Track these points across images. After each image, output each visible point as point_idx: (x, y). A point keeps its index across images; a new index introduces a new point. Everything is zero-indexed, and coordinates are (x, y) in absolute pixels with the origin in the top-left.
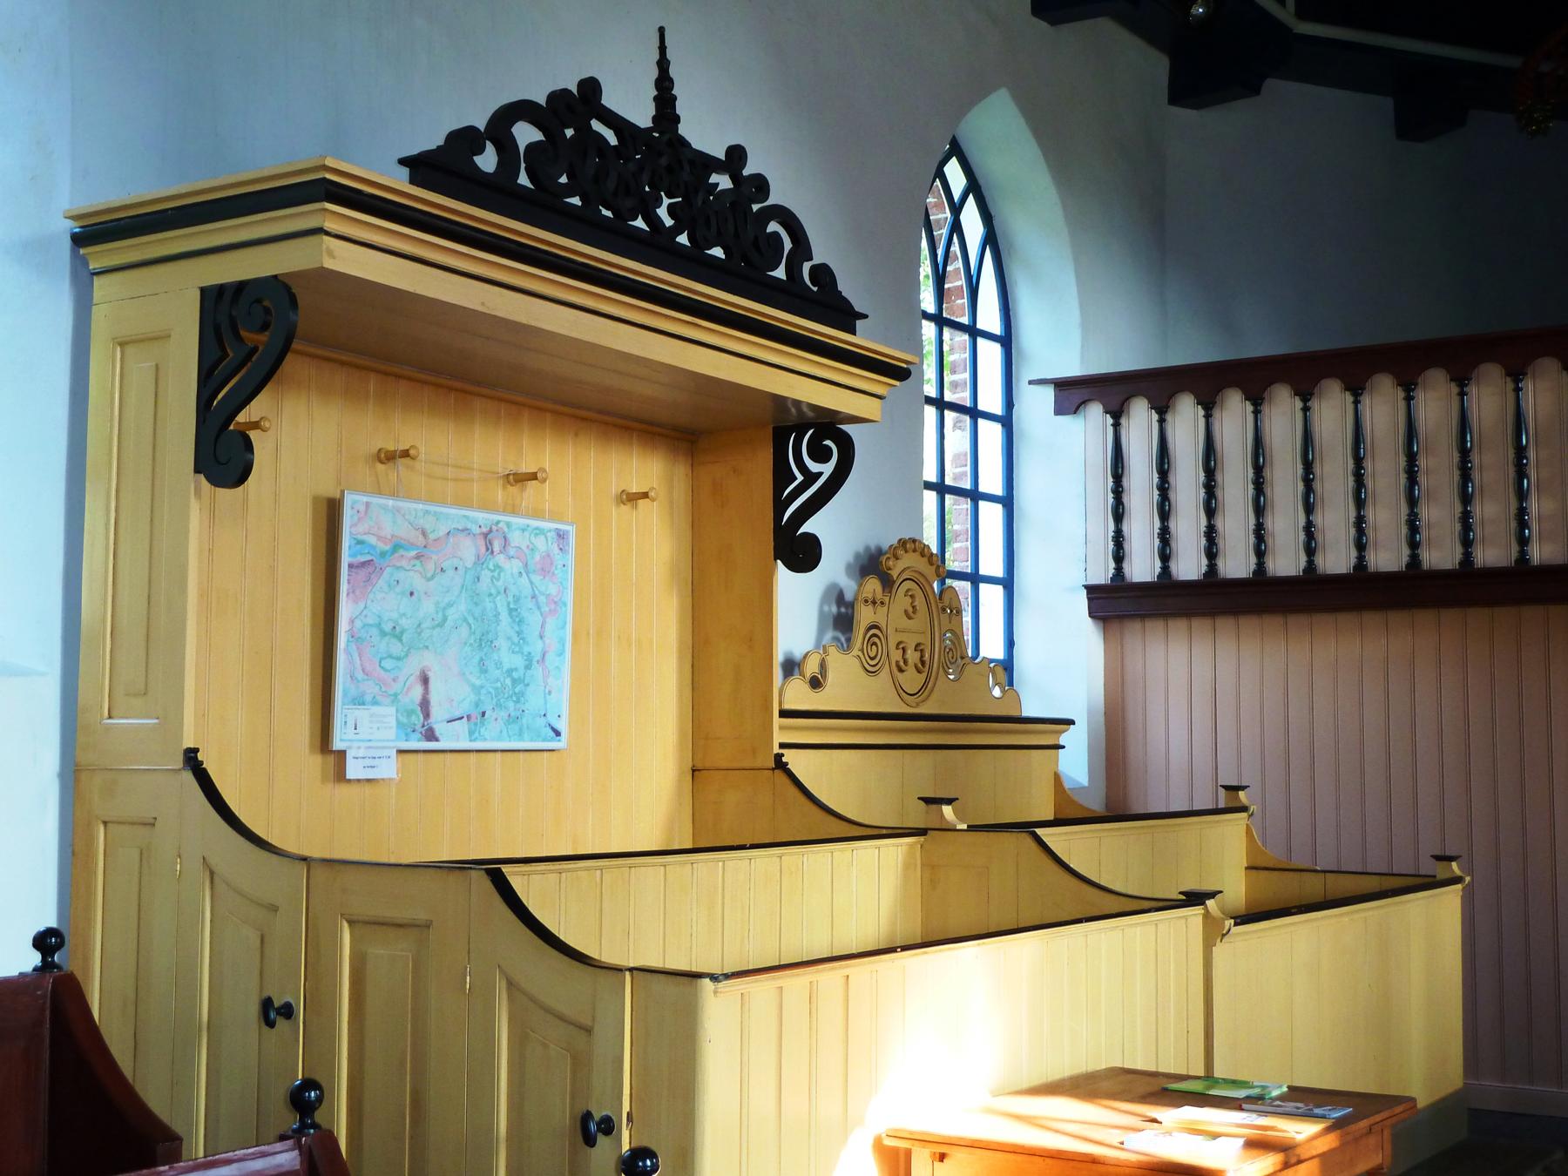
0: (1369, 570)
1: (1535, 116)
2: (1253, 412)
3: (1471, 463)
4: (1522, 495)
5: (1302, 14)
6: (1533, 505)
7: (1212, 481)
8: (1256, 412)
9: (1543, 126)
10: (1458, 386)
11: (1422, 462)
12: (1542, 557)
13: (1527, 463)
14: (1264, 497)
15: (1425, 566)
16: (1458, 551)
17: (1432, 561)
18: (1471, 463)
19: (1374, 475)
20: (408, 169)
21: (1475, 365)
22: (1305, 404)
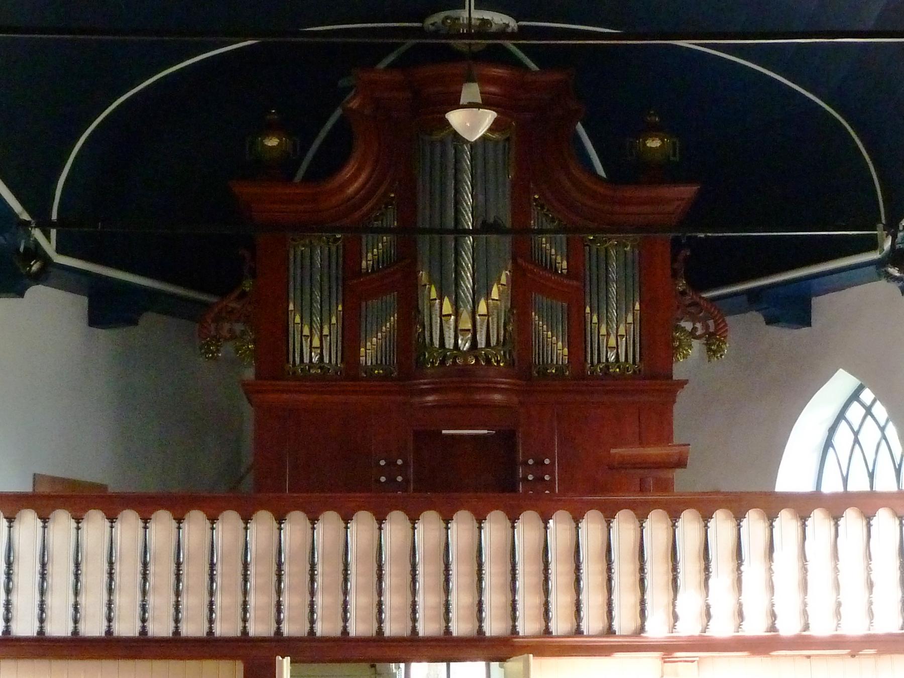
0: (215, 635)
1: (211, 348)
2: (76, 528)
3: (81, 570)
4: (212, 593)
5: (60, 250)
6: (218, 600)
7: (10, 570)
8: (44, 527)
9: (215, 354)
10: (8, 522)
11: (151, 568)
12: (222, 631)
13: (81, 573)
14: (216, 583)
15: (116, 634)
16: (172, 625)
17: (155, 630)
18: (81, 570)
19: (86, 575)
20: (841, 370)
21: (188, 510)
22: (10, 524)
